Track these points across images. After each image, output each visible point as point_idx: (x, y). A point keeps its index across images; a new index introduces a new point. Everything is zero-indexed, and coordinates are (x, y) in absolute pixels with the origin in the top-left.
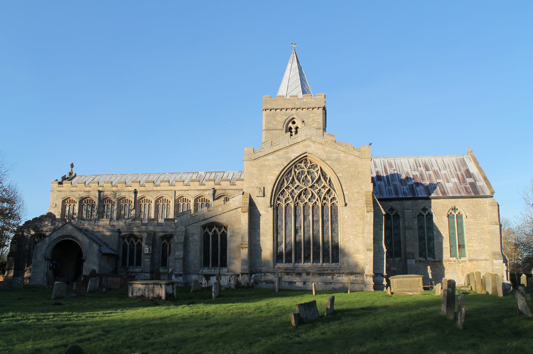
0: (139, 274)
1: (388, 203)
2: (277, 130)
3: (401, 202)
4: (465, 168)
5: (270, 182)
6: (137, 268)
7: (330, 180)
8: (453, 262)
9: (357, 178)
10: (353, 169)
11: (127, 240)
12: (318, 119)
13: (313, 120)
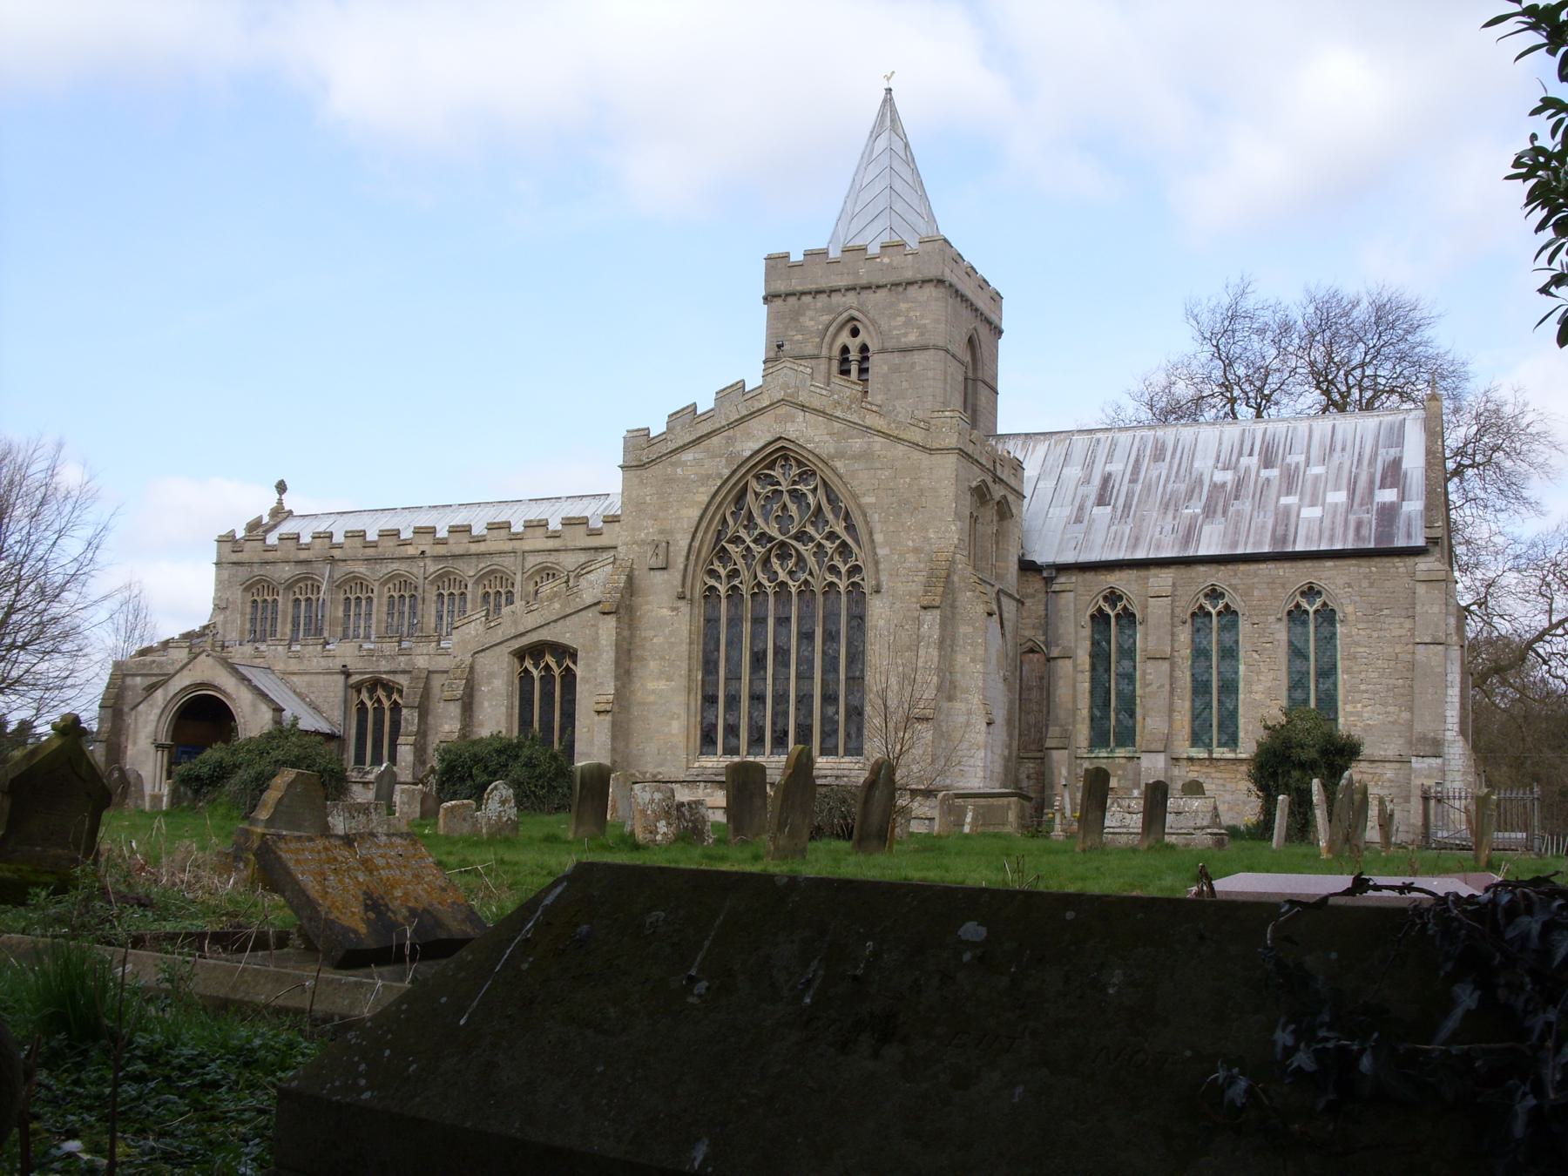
1: (1103, 577)
3: (1143, 573)
4: (1393, 452)
5: (685, 527)
7: (847, 513)
9: (915, 509)
10: (908, 480)
11: (367, 695)
12: (922, 316)
13: (908, 323)
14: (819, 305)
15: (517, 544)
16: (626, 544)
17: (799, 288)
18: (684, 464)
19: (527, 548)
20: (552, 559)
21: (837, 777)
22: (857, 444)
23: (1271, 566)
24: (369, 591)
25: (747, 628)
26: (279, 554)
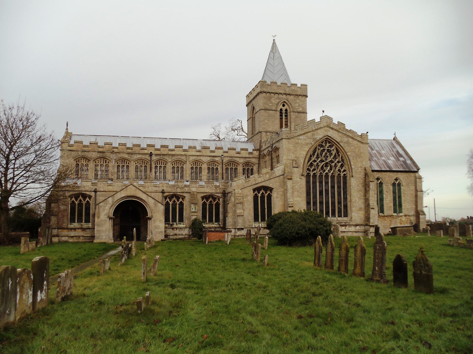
0: (184, 229)
2: (273, 110)
4: (396, 150)
6: (180, 224)
8: (395, 217)
13: (299, 106)
14: (276, 97)
15: (186, 153)
16: (285, 160)
17: (270, 91)
18: (300, 139)
19: (190, 154)
20: (198, 158)
21: (345, 223)
22: (345, 139)
23: (389, 173)
24: (127, 163)
25: (318, 184)
26: (90, 148)
